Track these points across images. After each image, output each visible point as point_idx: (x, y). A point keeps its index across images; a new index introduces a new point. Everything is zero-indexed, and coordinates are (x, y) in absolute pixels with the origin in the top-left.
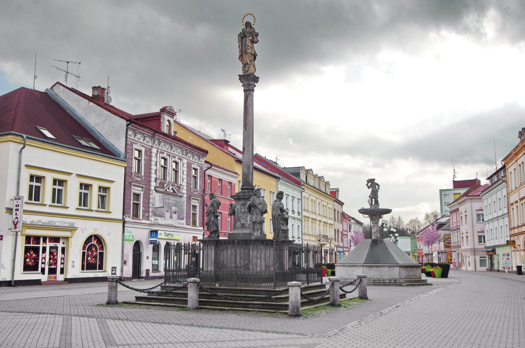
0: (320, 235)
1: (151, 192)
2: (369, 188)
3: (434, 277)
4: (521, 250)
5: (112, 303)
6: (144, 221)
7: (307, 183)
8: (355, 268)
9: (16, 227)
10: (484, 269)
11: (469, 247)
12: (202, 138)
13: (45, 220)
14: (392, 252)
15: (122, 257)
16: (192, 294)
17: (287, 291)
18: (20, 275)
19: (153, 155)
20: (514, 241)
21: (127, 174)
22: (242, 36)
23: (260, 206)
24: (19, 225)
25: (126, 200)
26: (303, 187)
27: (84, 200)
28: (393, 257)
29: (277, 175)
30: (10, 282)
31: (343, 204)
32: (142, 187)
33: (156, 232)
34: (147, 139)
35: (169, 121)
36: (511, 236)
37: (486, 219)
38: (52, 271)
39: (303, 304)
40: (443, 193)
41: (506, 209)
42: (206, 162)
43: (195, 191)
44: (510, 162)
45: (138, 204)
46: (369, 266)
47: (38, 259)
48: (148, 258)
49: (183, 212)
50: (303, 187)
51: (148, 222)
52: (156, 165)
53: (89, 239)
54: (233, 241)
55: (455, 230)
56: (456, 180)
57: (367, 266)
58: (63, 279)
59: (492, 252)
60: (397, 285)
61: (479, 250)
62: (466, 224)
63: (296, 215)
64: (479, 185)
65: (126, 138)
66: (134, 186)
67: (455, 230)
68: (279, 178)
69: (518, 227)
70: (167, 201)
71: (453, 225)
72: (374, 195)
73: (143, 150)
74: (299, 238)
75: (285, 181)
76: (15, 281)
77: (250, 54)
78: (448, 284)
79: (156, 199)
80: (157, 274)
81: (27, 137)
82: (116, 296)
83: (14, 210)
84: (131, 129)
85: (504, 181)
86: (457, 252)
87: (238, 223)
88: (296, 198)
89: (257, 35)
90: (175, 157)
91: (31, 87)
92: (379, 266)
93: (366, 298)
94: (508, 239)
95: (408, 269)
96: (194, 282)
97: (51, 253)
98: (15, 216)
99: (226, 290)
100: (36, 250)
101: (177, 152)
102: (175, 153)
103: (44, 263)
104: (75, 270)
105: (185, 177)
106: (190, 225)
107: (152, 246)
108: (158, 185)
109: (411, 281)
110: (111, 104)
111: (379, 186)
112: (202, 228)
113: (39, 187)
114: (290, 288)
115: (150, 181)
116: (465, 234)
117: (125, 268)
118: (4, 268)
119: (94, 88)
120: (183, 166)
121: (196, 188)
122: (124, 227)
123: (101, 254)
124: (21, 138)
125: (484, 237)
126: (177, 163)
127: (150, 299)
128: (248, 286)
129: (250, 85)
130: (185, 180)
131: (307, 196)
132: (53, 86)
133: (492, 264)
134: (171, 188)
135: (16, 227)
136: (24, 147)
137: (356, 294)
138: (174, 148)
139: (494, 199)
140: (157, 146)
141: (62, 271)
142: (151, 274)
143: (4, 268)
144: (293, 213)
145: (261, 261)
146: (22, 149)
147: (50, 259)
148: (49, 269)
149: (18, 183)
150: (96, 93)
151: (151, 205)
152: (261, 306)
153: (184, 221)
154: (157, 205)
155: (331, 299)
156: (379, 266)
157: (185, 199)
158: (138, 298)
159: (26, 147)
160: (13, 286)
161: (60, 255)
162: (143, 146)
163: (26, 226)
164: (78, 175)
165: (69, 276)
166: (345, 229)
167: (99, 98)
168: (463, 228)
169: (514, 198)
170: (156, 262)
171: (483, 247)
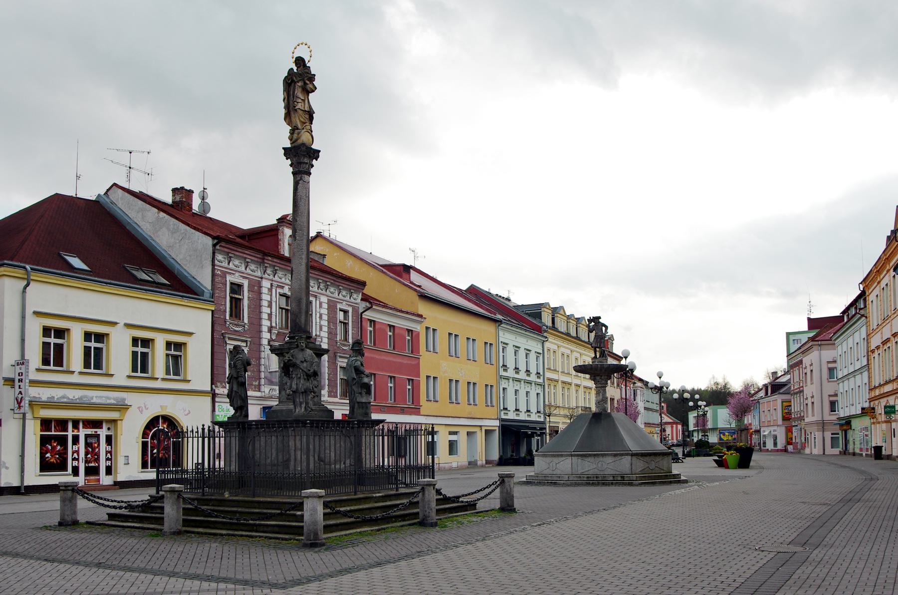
0: (577, 407)
3: (727, 467)
5: (68, 523)
7: (553, 327)
9: (20, 407)
10: (836, 451)
11: (815, 419)
12: (367, 262)
16: (171, 512)
17: (300, 506)
18: (34, 477)
19: (265, 290)
20: (873, 409)
22: (290, 82)
23: (305, 364)
24: (25, 404)
25: (216, 362)
26: (545, 334)
27: (141, 363)
29: (499, 317)
32: (246, 341)
34: (253, 266)
36: (871, 400)
38: (92, 471)
39: (327, 528)
40: (792, 338)
43: (345, 345)
44: (871, 285)
47: (66, 453)
50: (545, 334)
52: (270, 306)
53: (153, 422)
54: (273, 421)
56: (812, 317)
57: (578, 455)
58: (112, 483)
59: (846, 424)
60: (625, 484)
61: (831, 423)
62: (812, 384)
63: (533, 378)
65: (213, 265)
66: (230, 339)
71: (794, 387)
74: (539, 412)
76: (27, 488)
77: (301, 112)
81: (32, 269)
82: (75, 513)
83: (17, 381)
84: (221, 252)
85: (863, 316)
86: (799, 427)
91: (70, 192)
92: (598, 455)
94: (866, 405)
96: (179, 493)
97: (87, 445)
98: (18, 390)
99: (238, 503)
100: (63, 441)
103: (78, 460)
105: (325, 323)
106: (336, 396)
108: (274, 337)
110: (208, 215)
111: (606, 327)
115: (261, 332)
116: (809, 399)
118: (7, 468)
119: (175, 191)
120: (321, 307)
121: (346, 339)
122: (214, 402)
124: (22, 271)
128: (277, 495)
129: (301, 163)
130: (325, 329)
131: (555, 347)
132: (108, 190)
135: (20, 407)
136: (28, 285)
139: (850, 345)
140: (271, 277)
141: (109, 471)
143: (7, 468)
144: (528, 375)
146: (25, 288)
147: (87, 453)
149: (23, 340)
150: (178, 198)
151: (262, 368)
152: (276, 529)
156: (598, 455)
158: (111, 516)
159: (32, 284)
160: (22, 494)
164: (128, 326)
165: (120, 478)
168: (808, 390)
169: (876, 341)
171: (834, 418)
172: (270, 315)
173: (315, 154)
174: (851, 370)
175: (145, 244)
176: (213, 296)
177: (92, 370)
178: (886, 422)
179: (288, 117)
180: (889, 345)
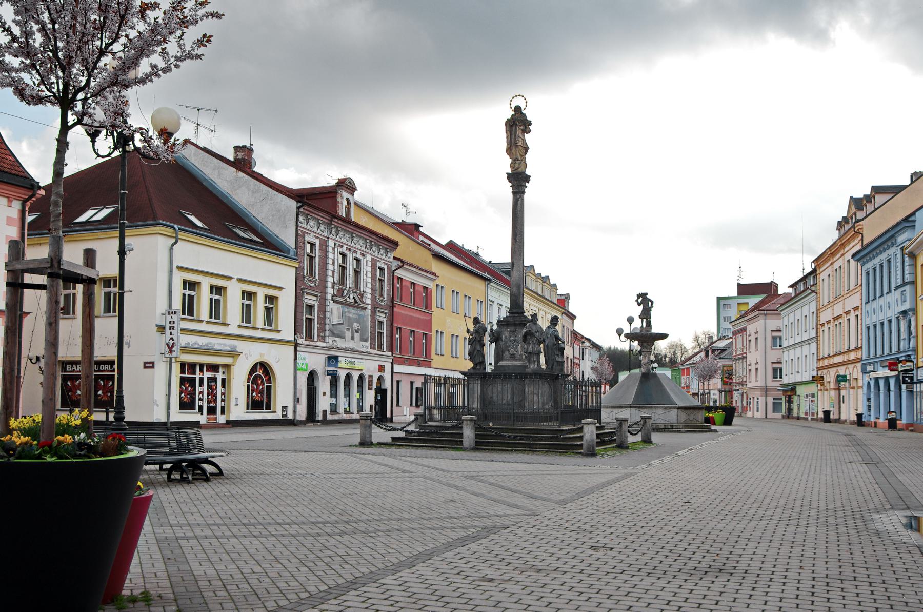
1: (327, 303)
2: (639, 305)
4: (831, 389)
5: (365, 443)
6: (319, 344)
8: (620, 410)
9: (171, 352)
10: (778, 415)
11: (758, 384)
12: (382, 220)
13: (202, 341)
14: (668, 390)
15: (295, 393)
16: (468, 433)
17: (581, 430)
19: (330, 249)
21: (299, 278)
27: (247, 313)
28: (669, 396)
30: (165, 423)
31: (575, 317)
32: (317, 296)
33: (336, 358)
35: (348, 199)
36: (819, 369)
37: (785, 344)
39: (598, 444)
40: (722, 302)
41: (815, 330)
42: (395, 258)
45: (311, 319)
46: (639, 408)
47: (195, 394)
48: (324, 394)
49: (366, 331)
51: (324, 344)
52: (333, 264)
53: (253, 369)
54: (500, 374)
55: (739, 359)
56: (742, 282)
59: (791, 391)
61: (774, 389)
64: (776, 295)
65: (297, 226)
66: (308, 294)
67: (739, 359)
68: (490, 280)
69: (829, 357)
70: (347, 314)
72: (646, 315)
73: (317, 242)
75: (498, 285)
78: (733, 432)
79: (335, 312)
80: (336, 417)
85: (813, 292)
86: (740, 392)
87: (507, 353)
88: (495, 303)
89: (530, 123)
90: (356, 252)
93: (651, 442)
94: (815, 373)
95: (688, 411)
96: (471, 420)
97: (209, 387)
100: (192, 382)
101: (359, 244)
102: (357, 246)
104: (239, 412)
105: (369, 280)
107: (329, 378)
109: (692, 427)
111: (652, 302)
112: (390, 354)
113: (193, 296)
114: (585, 426)
116: (753, 365)
117: (298, 407)
121: (382, 295)
123: (269, 388)
124: (172, 230)
125: (781, 370)
126: (344, 256)
127: (411, 440)
130: (369, 285)
133: (790, 410)
134: (352, 296)
135: (171, 352)
136: (176, 243)
137: (639, 438)
138: (341, 233)
139: (798, 316)
142: (329, 417)
145: (537, 397)
148: (208, 407)
150: (240, 156)
151: (327, 321)
153: (368, 344)
154: (336, 320)
155: (619, 441)
157: (368, 312)
159: (180, 242)
161: (220, 389)
162: (317, 237)
163: (186, 350)
164: (240, 280)
165: (232, 418)
166: (577, 355)
167: (243, 161)
168: (752, 357)
169: (825, 316)
170: (334, 401)
171: (778, 384)
172: (333, 272)
173: (527, 179)
174: (798, 340)
175: (225, 201)
176: (296, 254)
177: (186, 316)
178: (835, 389)
179: (509, 151)
180: (840, 320)
